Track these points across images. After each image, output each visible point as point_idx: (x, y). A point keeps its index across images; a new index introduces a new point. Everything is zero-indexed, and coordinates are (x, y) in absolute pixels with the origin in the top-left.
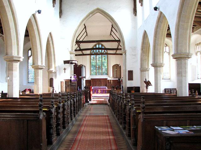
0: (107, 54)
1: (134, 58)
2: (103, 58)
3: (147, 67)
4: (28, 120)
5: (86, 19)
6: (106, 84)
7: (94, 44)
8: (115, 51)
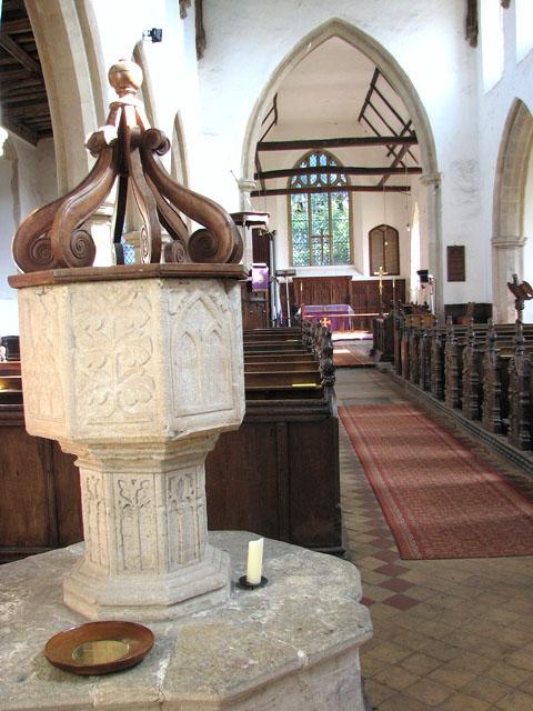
0: (349, 188)
1: (467, 202)
2: (335, 205)
3: (517, 234)
4: (288, 423)
5: (295, 61)
6: (348, 297)
7: (302, 152)
8: (377, 179)
